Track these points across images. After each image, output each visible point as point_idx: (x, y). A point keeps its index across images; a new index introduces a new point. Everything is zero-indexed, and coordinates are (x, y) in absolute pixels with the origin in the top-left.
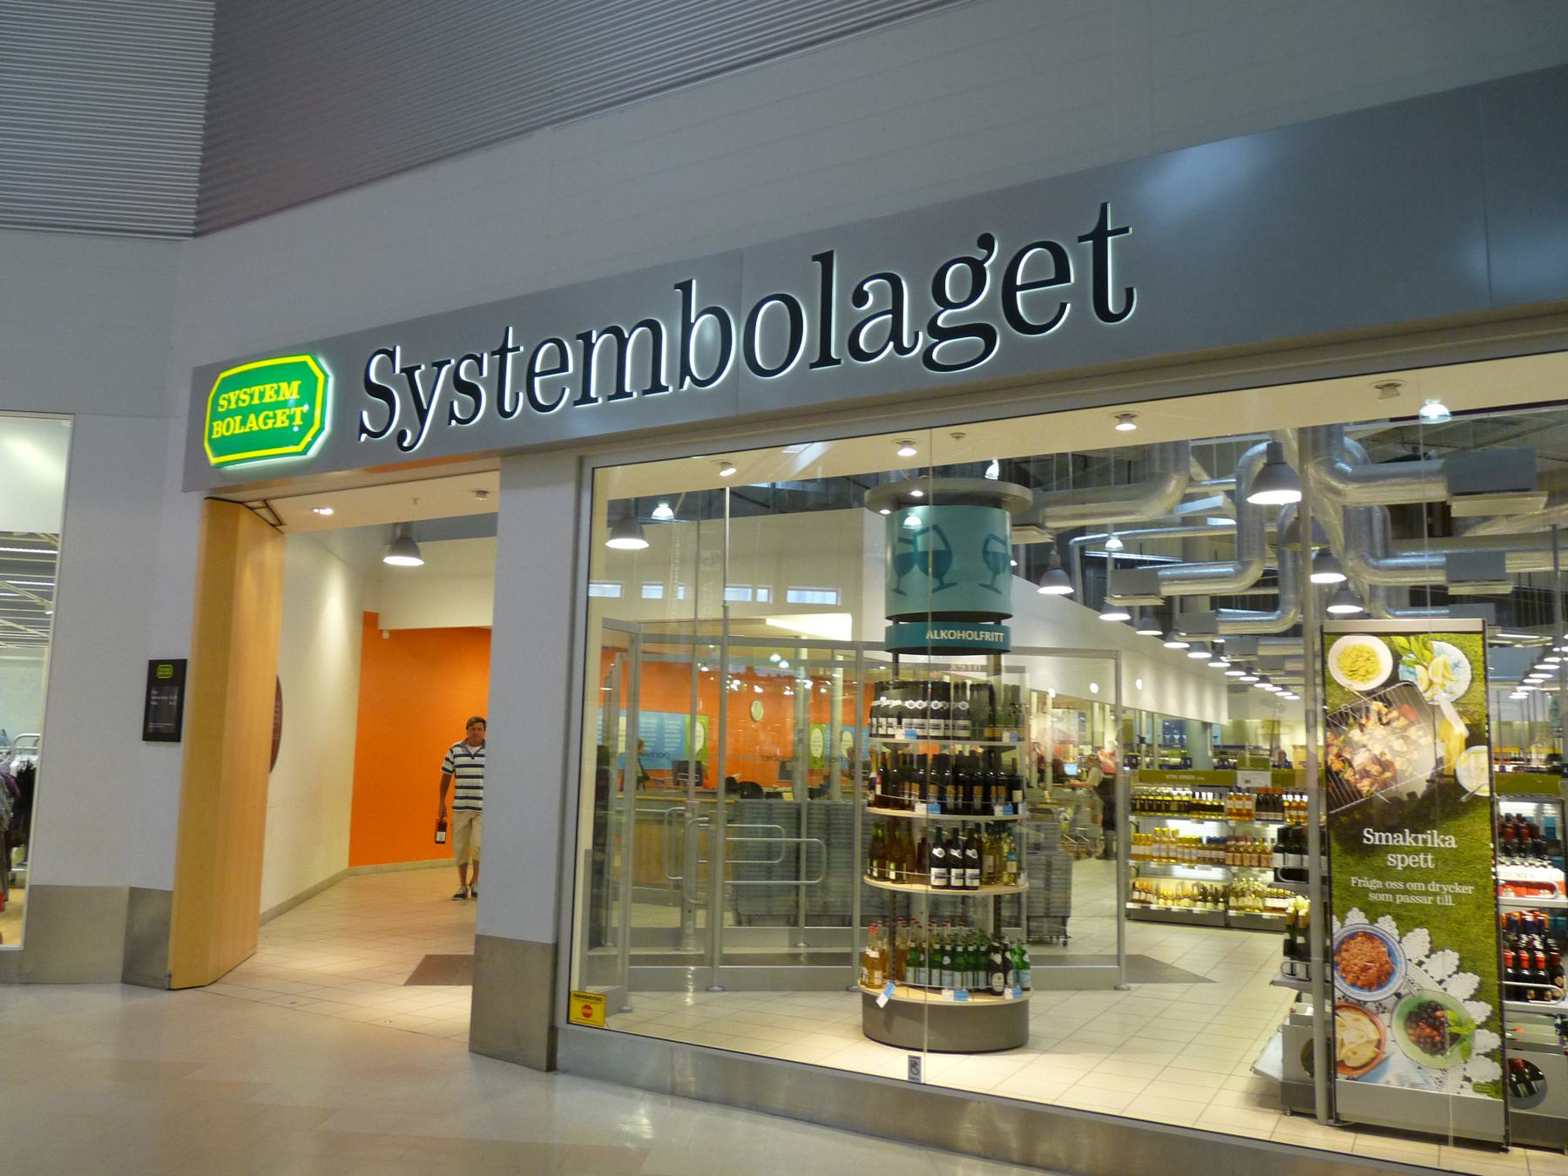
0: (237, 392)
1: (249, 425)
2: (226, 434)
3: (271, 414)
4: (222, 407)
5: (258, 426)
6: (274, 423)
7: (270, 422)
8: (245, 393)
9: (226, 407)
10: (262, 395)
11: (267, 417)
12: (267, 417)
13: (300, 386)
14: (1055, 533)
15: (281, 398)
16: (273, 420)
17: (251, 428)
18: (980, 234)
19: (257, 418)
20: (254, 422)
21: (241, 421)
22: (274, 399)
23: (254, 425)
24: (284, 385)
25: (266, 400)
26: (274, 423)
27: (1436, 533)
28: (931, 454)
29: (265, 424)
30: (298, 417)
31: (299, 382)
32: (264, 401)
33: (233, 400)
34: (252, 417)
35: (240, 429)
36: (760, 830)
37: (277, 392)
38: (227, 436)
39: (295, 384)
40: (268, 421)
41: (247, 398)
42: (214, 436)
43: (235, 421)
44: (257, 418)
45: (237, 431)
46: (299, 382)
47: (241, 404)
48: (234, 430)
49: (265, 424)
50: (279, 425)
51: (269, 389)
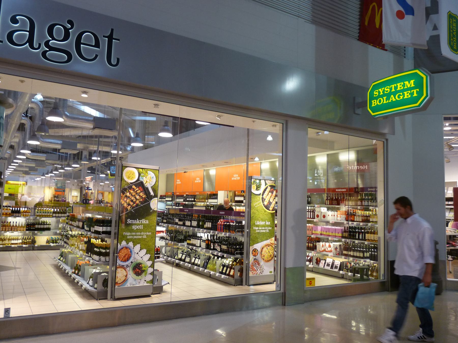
0: (383, 89)
1: (391, 99)
5: (395, 99)
6: (404, 96)
7: (401, 97)
12: (400, 95)
15: (406, 87)
26: (403, 97)
33: (381, 91)
35: (386, 101)
42: (373, 105)
47: (385, 92)
48: (383, 101)
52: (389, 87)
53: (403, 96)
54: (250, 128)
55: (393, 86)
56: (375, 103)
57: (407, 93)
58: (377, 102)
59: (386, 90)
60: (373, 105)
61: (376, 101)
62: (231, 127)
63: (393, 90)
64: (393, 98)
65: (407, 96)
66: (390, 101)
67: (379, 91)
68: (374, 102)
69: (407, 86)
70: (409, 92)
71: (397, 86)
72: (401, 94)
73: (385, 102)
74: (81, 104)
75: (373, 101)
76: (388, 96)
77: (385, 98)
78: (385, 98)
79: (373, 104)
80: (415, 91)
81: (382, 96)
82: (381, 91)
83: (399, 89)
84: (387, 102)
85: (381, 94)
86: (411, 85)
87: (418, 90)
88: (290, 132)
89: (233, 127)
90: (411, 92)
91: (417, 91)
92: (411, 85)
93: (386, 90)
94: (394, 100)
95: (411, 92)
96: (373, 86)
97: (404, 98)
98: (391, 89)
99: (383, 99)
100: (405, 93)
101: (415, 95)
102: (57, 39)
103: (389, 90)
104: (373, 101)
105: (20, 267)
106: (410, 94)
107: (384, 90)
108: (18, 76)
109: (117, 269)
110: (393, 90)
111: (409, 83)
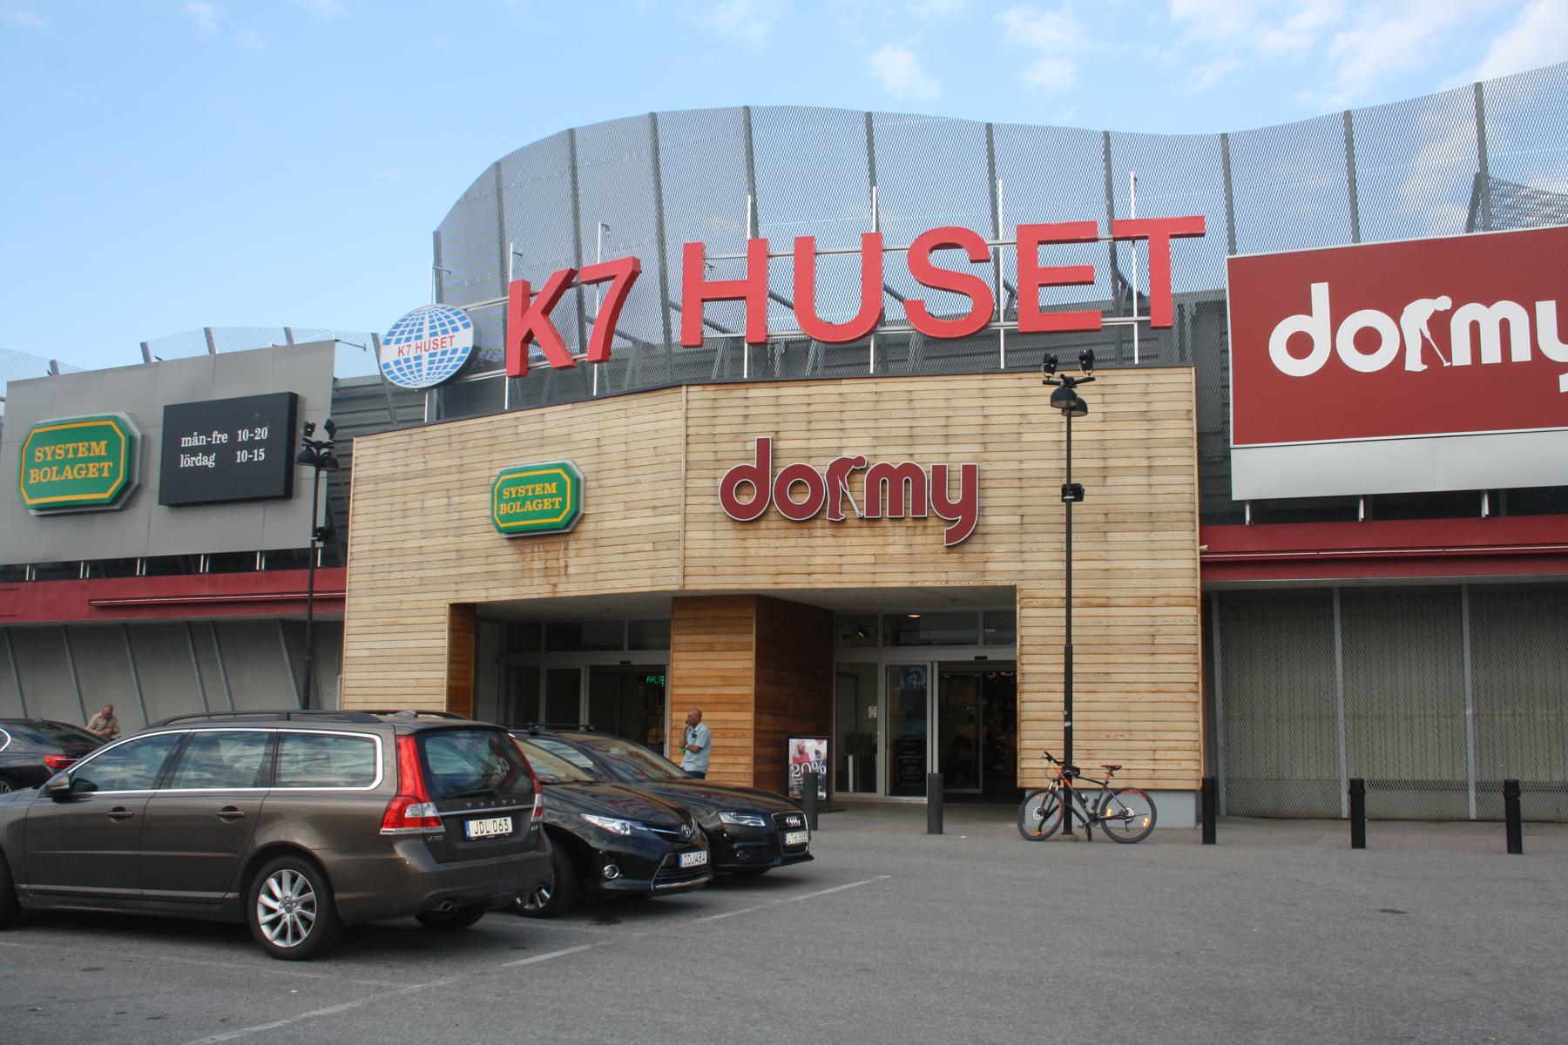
0: (53, 447)
1: (65, 474)
2: (43, 480)
3: (84, 466)
4: (39, 458)
5: (73, 475)
6: (87, 474)
7: (540, 506)
8: (60, 448)
9: (42, 459)
10: (76, 451)
11: (81, 469)
12: (81, 469)
13: (106, 445)
14: (302, 902)
15: (92, 454)
16: (85, 472)
17: (66, 477)
18: (1501, 318)
19: (72, 471)
20: (69, 471)
21: (57, 470)
22: (86, 455)
23: (530, 507)
24: (94, 444)
25: (537, 493)
26: (87, 474)
27: (332, 488)
28: (355, 346)
29: (79, 474)
30: (106, 469)
31: (106, 442)
32: (78, 456)
33: (49, 453)
34: (528, 502)
35: (57, 477)
36: (266, 737)
37: (89, 449)
38: (44, 483)
39: (103, 444)
40: (82, 472)
41: (62, 452)
42: (32, 481)
43: (52, 470)
44: (72, 471)
45: (54, 479)
46: (106, 442)
47: (57, 457)
48: (51, 477)
49: (80, 474)
50: (545, 508)
51: (538, 487)
52: (63, 446)
54: (1116, 126)
55: (530, 486)
56: (36, 476)
58: (39, 475)
59: (58, 452)
60: (32, 481)
61: (37, 471)
62: (650, 134)
63: (530, 494)
64: (529, 507)
65: (93, 474)
67: (45, 451)
68: (35, 473)
70: (97, 464)
71: (78, 447)
74: (382, 922)
75: (32, 471)
76: (523, 500)
79: (32, 479)
82: (49, 453)
83: (537, 493)
85: (514, 496)
87: (560, 499)
89: (873, 182)
91: (109, 466)
93: (520, 491)
94: (531, 509)
96: (118, 436)
98: (527, 491)
99: (516, 506)
104: (32, 471)
107: (517, 492)
108: (952, 291)
110: (530, 494)
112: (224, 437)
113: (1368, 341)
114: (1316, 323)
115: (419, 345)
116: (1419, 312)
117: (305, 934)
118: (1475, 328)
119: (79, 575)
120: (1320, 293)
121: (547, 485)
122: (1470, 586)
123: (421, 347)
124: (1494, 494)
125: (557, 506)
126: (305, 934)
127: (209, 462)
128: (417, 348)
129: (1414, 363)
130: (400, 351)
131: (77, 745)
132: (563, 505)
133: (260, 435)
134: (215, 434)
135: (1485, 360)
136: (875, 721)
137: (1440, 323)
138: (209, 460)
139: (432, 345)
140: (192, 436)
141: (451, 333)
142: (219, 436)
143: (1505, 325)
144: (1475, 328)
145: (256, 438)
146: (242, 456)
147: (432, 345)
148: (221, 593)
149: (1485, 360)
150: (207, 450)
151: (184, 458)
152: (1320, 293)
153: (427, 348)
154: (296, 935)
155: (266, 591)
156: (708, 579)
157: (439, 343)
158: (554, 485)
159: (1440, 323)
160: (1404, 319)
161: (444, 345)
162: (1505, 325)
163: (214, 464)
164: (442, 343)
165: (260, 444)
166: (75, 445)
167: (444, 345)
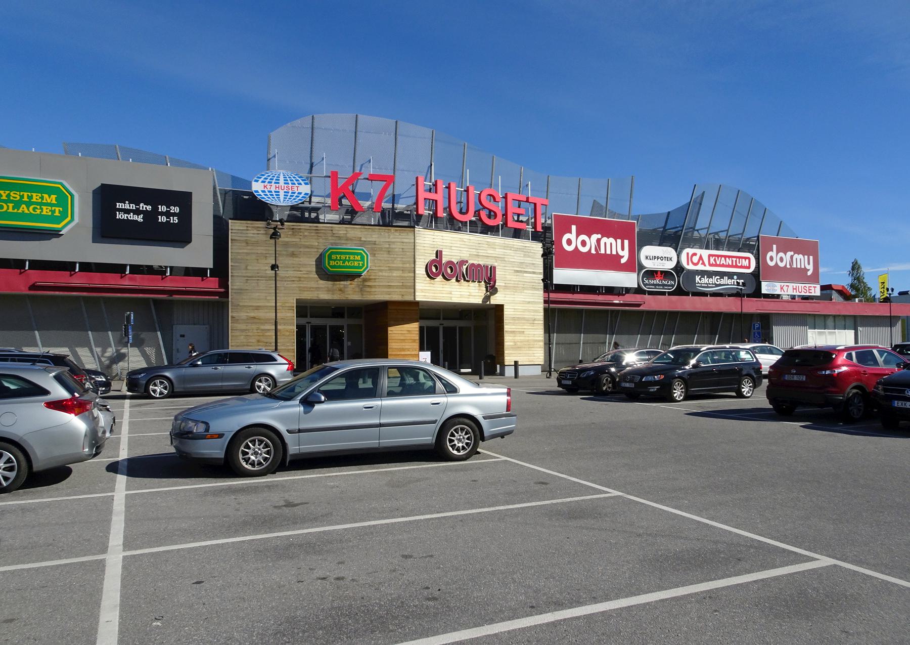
0: (7, 192)
1: (21, 209)
6: (42, 211)
7: (353, 264)
47: (11, 198)
53: (40, 210)
57: (47, 209)
63: (347, 258)
66: (20, 211)
69: (46, 200)
70: (50, 208)
71: (32, 195)
72: (38, 207)
73: (341, 264)
76: (344, 261)
77: (341, 262)
78: (341, 262)
80: (57, 209)
81: (339, 260)
83: (34, 200)
84: (16, 211)
86: (52, 201)
88: (740, 311)
90: (52, 208)
92: (52, 201)
94: (27, 211)
95: (52, 208)
96: (67, 195)
97: (42, 213)
100: (44, 208)
101: (57, 214)
102: (11, 446)
103: (18, 198)
105: (306, 502)
106: (50, 211)
109: (37, 466)
111: (49, 198)
112: (149, 208)
113: (584, 243)
114: (572, 236)
115: (795, 287)
116: (595, 237)
117: (675, 387)
118: (605, 243)
119: (25, 267)
120: (574, 228)
121: (356, 256)
122: (611, 310)
123: (279, 187)
124: (581, 286)
125: (361, 265)
126: (744, 382)
127: (140, 218)
128: (793, 289)
129: (593, 252)
130: (265, 187)
131: (697, 351)
132: (363, 265)
133: (174, 210)
134: (141, 205)
135: (613, 253)
136: (348, 341)
137: (598, 241)
138: (138, 218)
139: (803, 290)
140: (125, 203)
141: (297, 185)
142: (144, 206)
143: (611, 244)
144: (605, 243)
145: (171, 211)
146: (162, 219)
147: (803, 290)
148: (145, 285)
149: (613, 253)
150: (137, 212)
151: (119, 214)
152: (574, 228)
153: (800, 291)
154: (745, 382)
155: (126, 283)
156: (466, 299)
157: (807, 289)
158: (359, 256)
159: (598, 241)
160: (591, 239)
161: (810, 291)
162: (611, 244)
163: (142, 220)
164: (809, 290)
165: (174, 215)
166: (29, 194)
167: (810, 291)
